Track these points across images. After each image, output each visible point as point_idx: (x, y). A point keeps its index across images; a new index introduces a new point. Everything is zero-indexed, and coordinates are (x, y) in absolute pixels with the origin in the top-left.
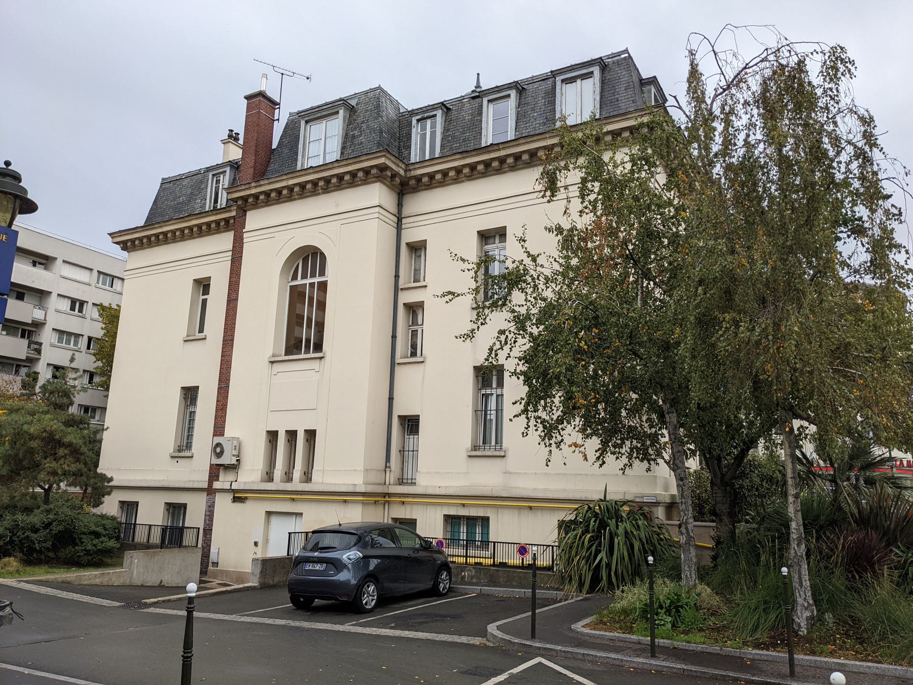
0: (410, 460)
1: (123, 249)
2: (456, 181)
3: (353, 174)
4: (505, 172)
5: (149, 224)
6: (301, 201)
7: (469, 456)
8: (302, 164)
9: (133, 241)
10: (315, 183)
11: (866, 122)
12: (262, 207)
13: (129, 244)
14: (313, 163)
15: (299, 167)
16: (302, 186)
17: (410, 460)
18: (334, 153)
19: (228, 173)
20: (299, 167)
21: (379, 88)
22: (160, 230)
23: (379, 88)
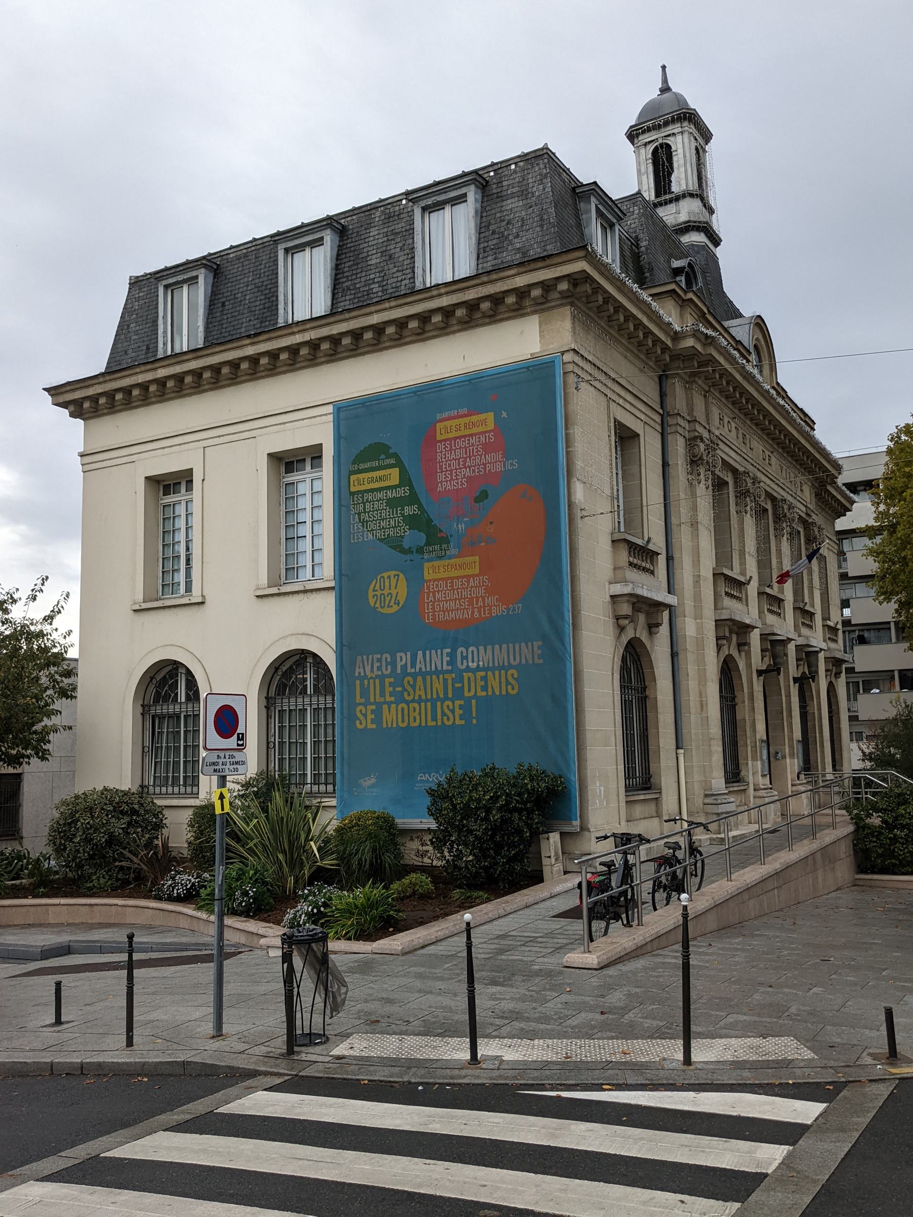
0: (688, 155)
1: (72, 415)
2: (444, 330)
3: (356, 335)
4: (454, 332)
5: (114, 369)
6: (270, 380)
7: (134, 611)
8: (165, 351)
9: (94, 399)
10: (314, 345)
11: (73, 881)
12: (190, 395)
13: (86, 405)
14: (302, 314)
15: (281, 322)
16: (293, 350)
17: (688, 155)
18: (321, 306)
19: (201, 280)
20: (281, 322)
21: (595, 183)
22: (149, 376)
23: (595, 183)
